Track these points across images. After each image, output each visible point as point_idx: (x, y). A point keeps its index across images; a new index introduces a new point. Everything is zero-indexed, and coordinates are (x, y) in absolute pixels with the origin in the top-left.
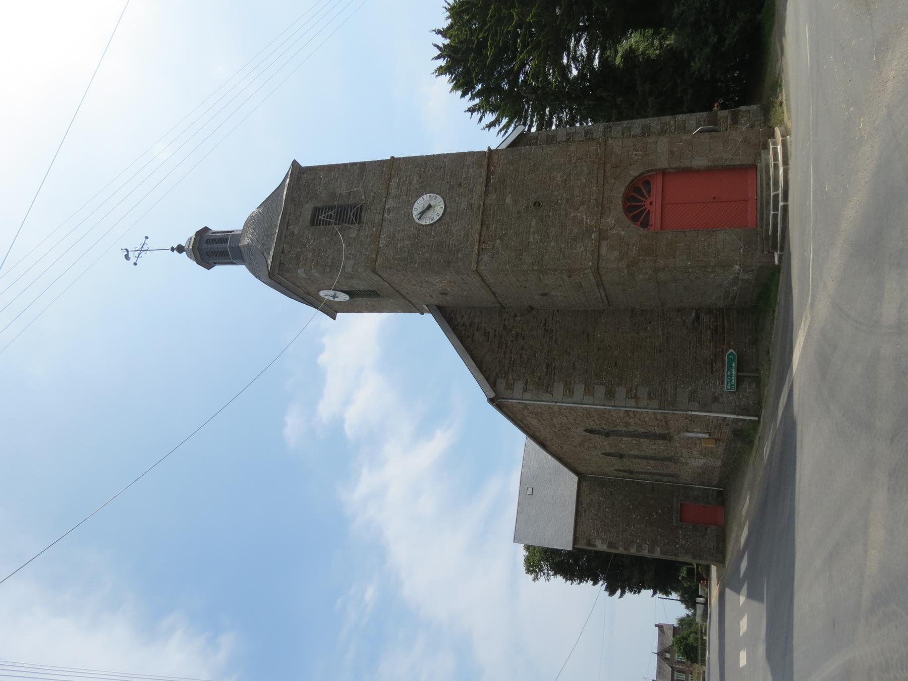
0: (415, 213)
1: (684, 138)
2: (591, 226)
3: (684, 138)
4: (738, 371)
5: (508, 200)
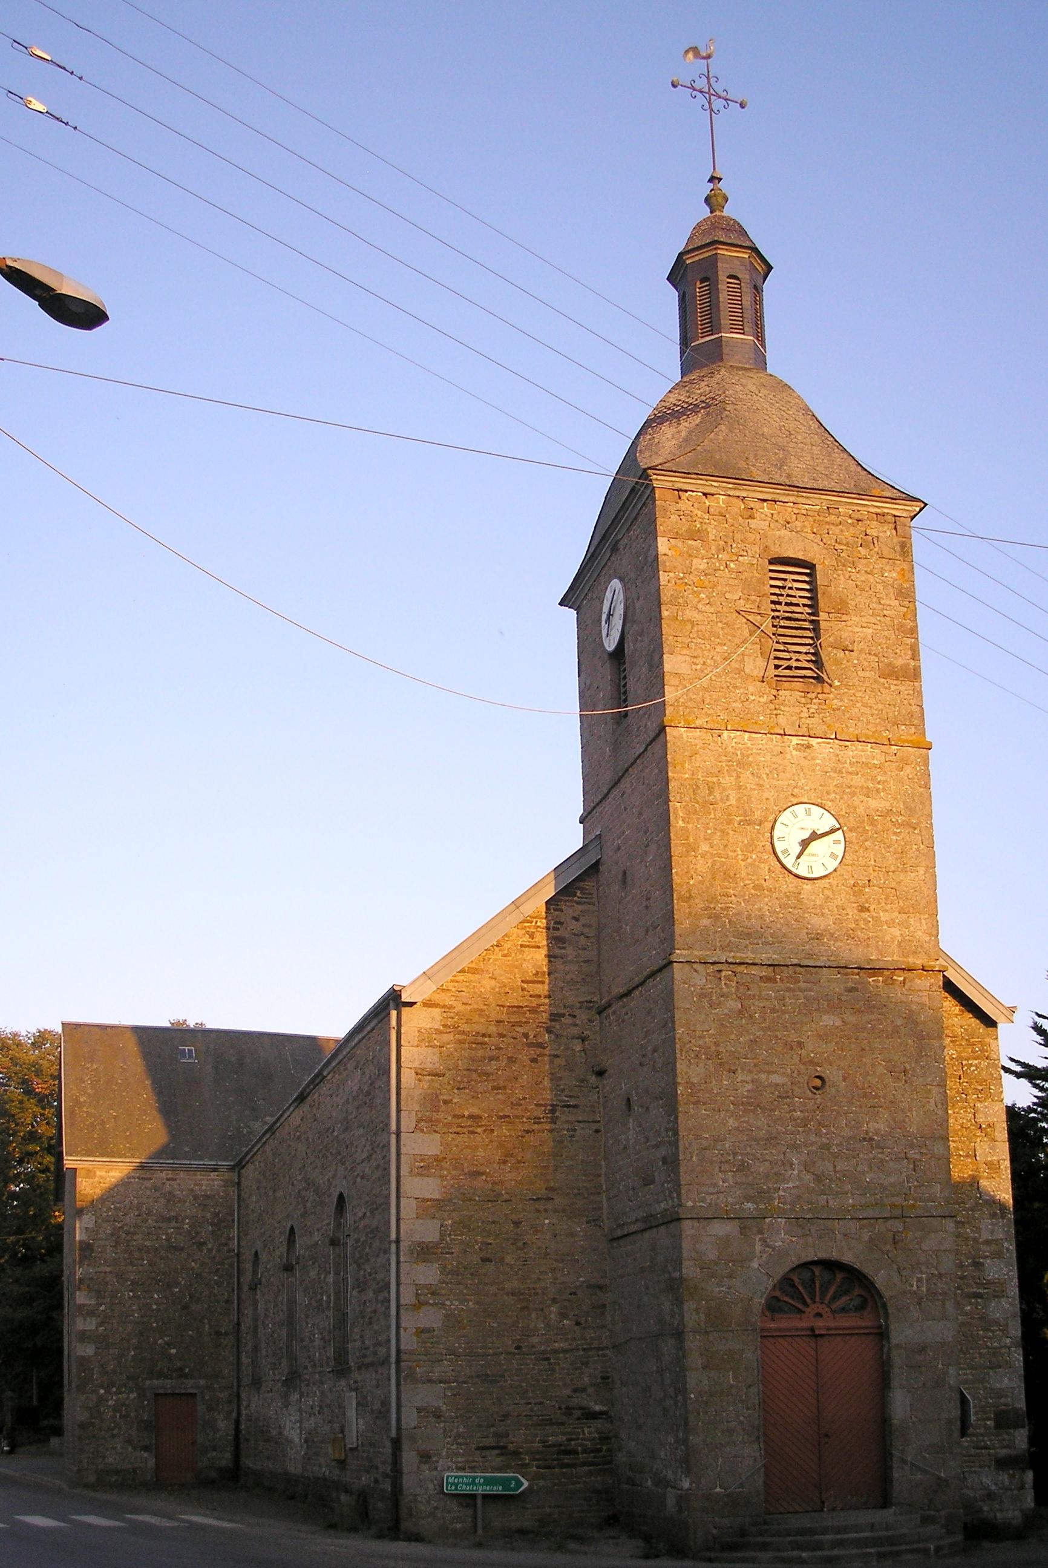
2: (771, 1199)
4: (485, 1496)
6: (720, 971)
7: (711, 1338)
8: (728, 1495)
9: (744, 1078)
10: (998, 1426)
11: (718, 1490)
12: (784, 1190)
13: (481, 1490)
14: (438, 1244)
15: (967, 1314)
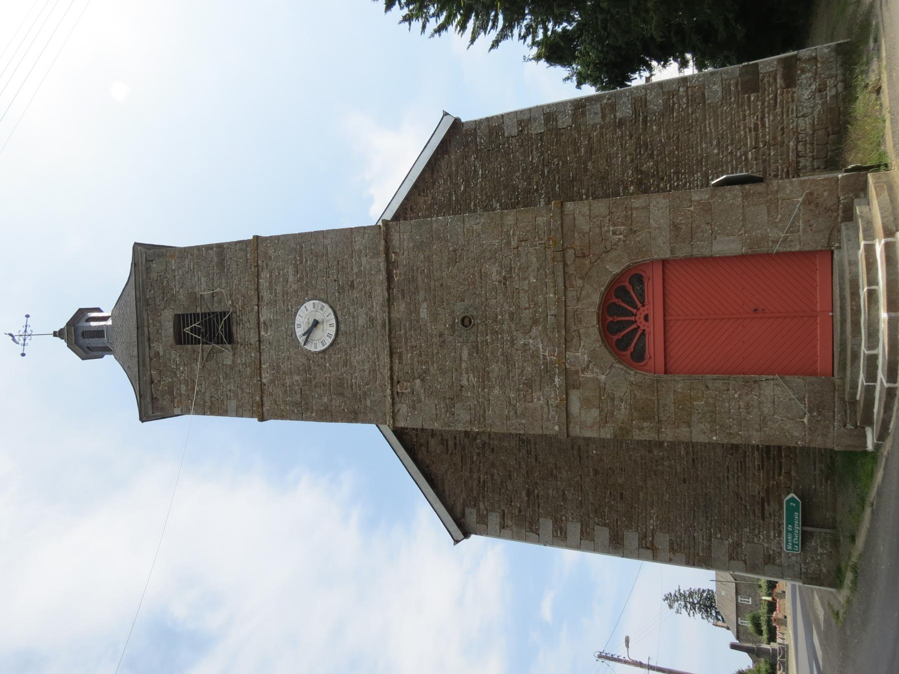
0: (299, 332)
1: (696, 198)
2: (552, 362)
3: (696, 198)
5: (424, 313)
6: (398, 393)
7: (665, 418)
8: (810, 411)
9: (465, 380)
10: (755, 90)
11: (806, 420)
12: (545, 351)
13: (798, 528)
14: (610, 529)
15: (660, 130)
